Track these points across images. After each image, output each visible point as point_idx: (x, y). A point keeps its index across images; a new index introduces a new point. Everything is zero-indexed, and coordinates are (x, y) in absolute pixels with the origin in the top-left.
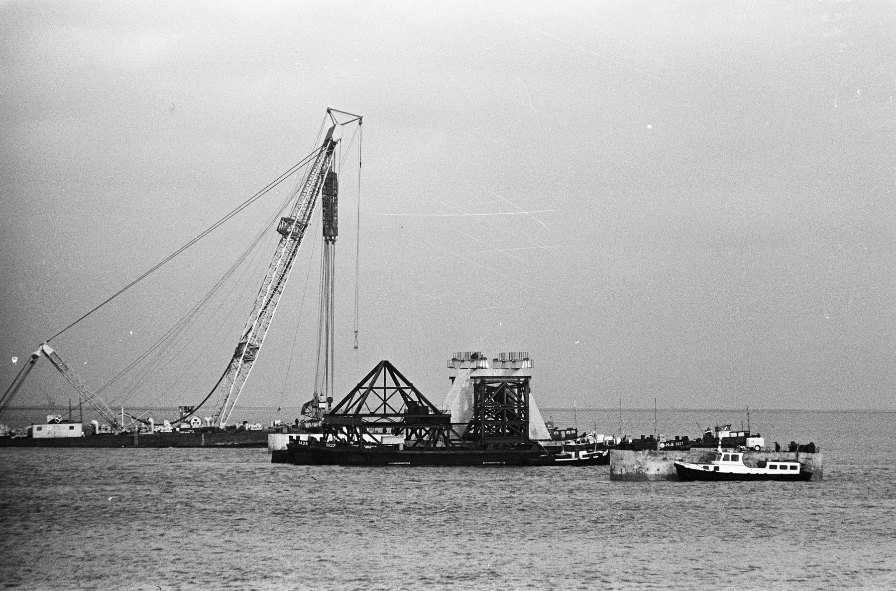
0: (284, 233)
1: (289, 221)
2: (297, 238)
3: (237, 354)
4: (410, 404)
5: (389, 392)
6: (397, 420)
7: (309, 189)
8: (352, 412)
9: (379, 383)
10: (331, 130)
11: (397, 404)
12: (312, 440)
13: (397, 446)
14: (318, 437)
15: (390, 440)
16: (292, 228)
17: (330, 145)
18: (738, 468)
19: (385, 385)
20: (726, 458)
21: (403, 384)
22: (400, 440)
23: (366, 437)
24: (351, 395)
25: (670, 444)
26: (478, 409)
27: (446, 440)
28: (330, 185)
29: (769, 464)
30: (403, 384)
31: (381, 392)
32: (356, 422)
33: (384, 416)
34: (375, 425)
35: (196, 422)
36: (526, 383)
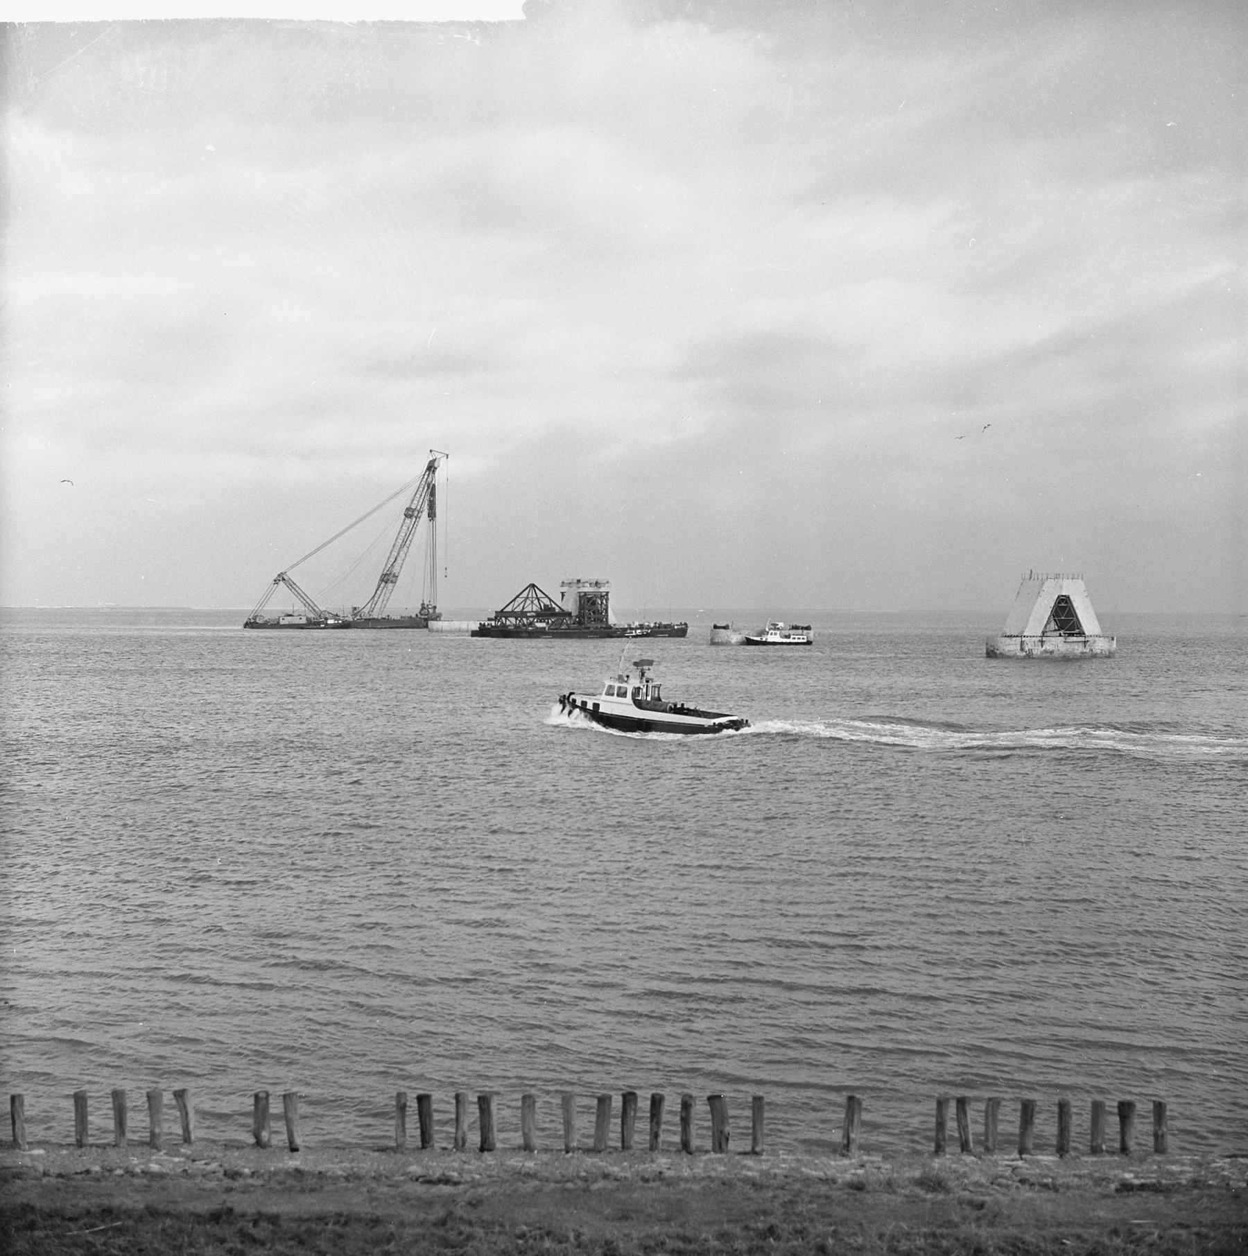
17: (431, 468)
18: (778, 639)
28: (432, 491)
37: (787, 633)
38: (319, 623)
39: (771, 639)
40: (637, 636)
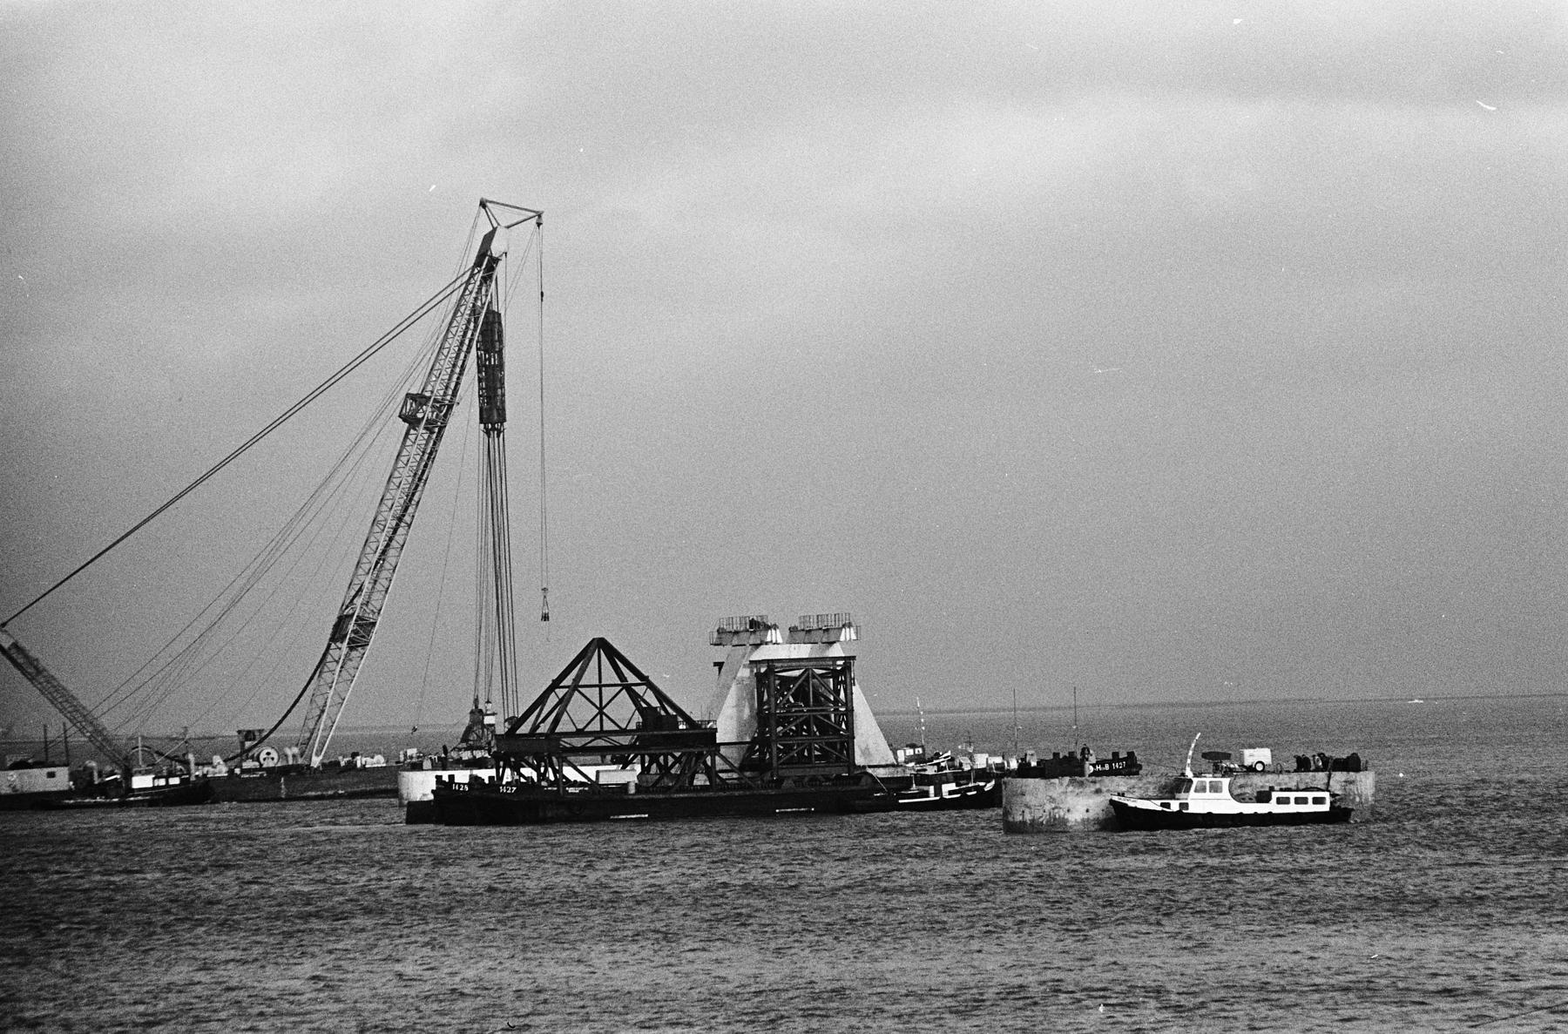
0: (411, 421)
1: (419, 399)
2: (436, 428)
3: (337, 634)
4: (647, 712)
5: (608, 693)
6: (625, 740)
7: (453, 343)
8: (544, 728)
9: (590, 676)
10: (488, 238)
11: (623, 712)
12: (475, 780)
13: (625, 786)
14: (485, 774)
15: (613, 775)
16: (427, 412)
17: (487, 262)
18: (1224, 804)
19: (600, 681)
20: (1202, 789)
21: (632, 678)
22: (630, 776)
23: (569, 772)
24: (542, 700)
25: (1103, 766)
26: (763, 718)
27: (710, 772)
28: (490, 333)
29: (1275, 795)
30: (632, 678)
31: (593, 694)
32: (550, 748)
33: (601, 734)
34: (584, 750)
35: (269, 757)
36: (847, 668)
37: (1260, 782)
38: (104, 789)
39: (1198, 803)
40: (943, 804)
